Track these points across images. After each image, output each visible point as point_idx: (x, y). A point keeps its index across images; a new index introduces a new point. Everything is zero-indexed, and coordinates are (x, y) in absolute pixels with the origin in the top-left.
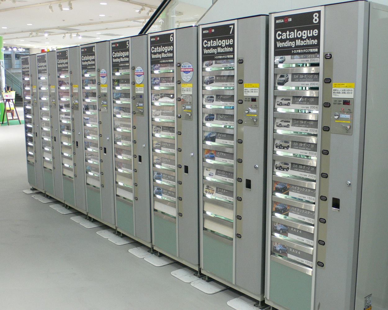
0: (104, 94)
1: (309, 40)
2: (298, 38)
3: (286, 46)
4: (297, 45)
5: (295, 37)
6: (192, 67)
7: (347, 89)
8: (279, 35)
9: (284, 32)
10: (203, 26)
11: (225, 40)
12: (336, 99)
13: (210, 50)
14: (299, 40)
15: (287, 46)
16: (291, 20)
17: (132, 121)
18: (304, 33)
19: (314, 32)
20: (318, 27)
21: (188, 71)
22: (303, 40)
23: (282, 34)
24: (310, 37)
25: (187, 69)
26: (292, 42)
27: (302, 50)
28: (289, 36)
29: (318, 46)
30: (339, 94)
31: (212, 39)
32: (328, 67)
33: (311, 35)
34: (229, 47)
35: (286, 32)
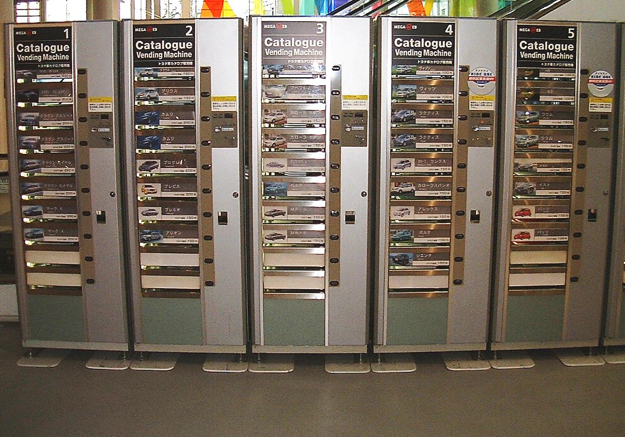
0: (100, 114)
1: (182, 53)
2: (166, 50)
3: (150, 57)
4: (165, 57)
5: (546, 49)
6: (611, 77)
7: (229, 102)
8: (140, 45)
9: (417, 40)
10: (394, 18)
11: (177, 43)
12: (216, 113)
13: (28, 56)
14: (551, 53)
15: (534, 57)
16: (416, 28)
17: (190, 144)
18: (435, 44)
19: (447, 44)
20: (574, 42)
21: (603, 83)
22: (557, 53)
23: (403, 41)
24: (183, 49)
25: (483, 77)
26: (158, 53)
27: (172, 63)
28: (538, 47)
29: (70, 61)
30: (350, 106)
31: (152, 40)
32: (83, 83)
33: (566, 49)
34: (566, 54)
35: (150, 43)
